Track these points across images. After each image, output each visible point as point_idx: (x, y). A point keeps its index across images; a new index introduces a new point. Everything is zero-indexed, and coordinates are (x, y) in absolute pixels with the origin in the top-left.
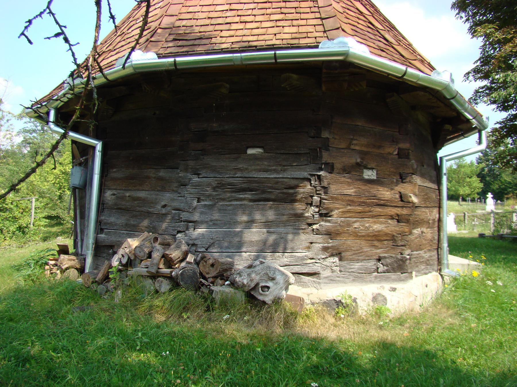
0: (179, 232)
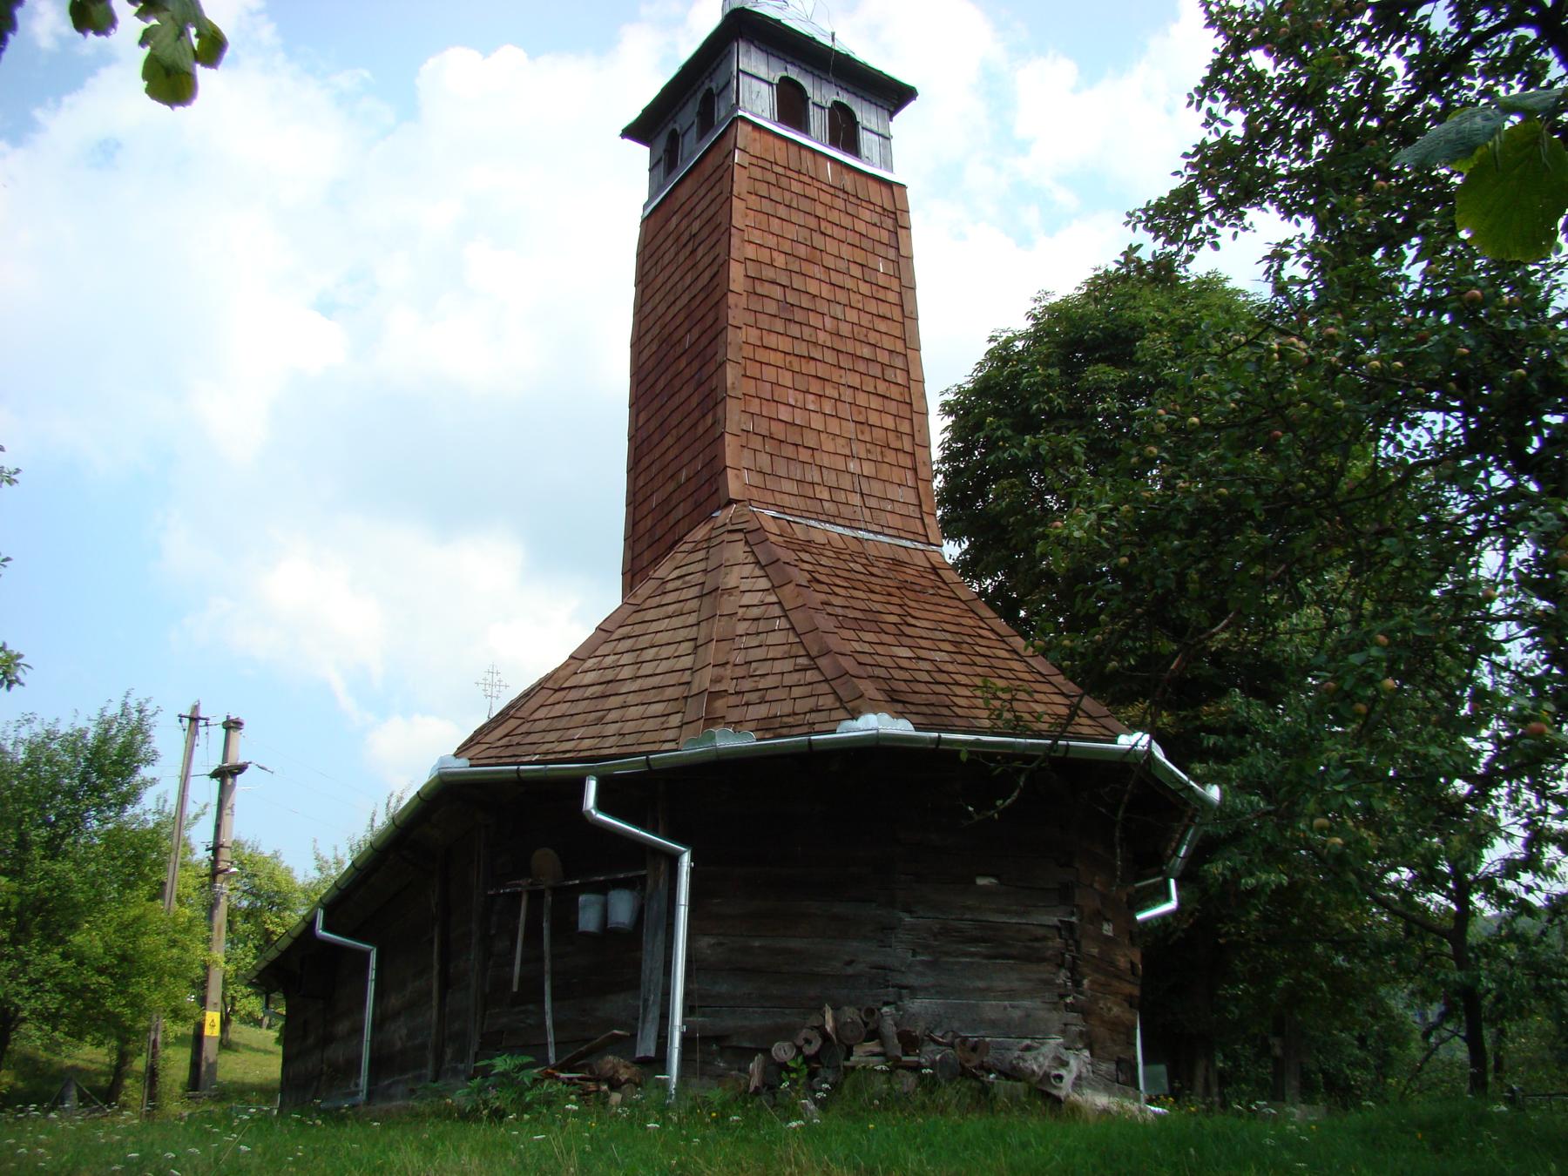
0: (886, 1004)
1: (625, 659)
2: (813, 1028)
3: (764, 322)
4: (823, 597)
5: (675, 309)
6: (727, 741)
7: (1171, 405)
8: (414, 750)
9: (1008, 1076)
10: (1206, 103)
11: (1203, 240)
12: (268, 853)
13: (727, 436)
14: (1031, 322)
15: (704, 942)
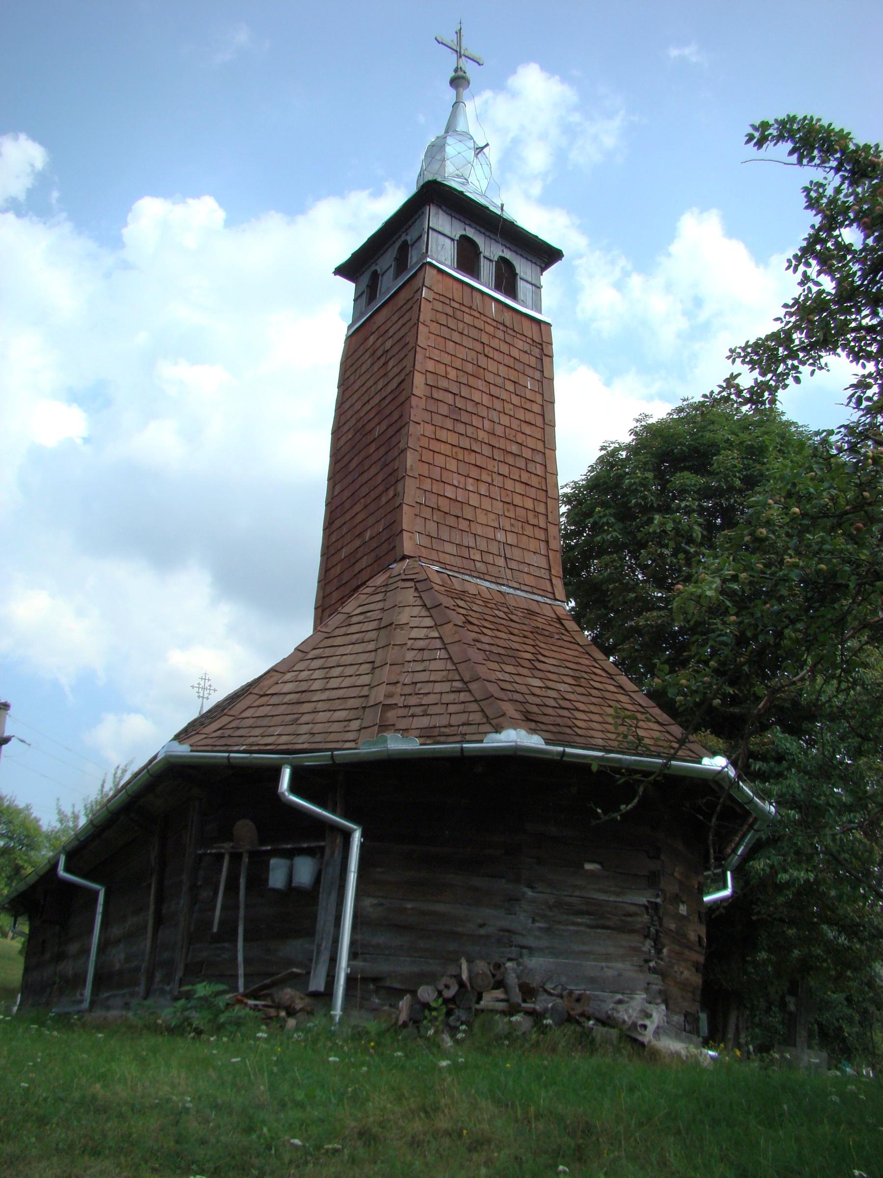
0: (510, 960)
1: (317, 674)
2: (452, 976)
3: (438, 420)
4: (474, 635)
5: (368, 407)
6: (397, 744)
7: (777, 497)
8: (137, 737)
9: (604, 1023)
10: (802, 268)
11: (788, 374)
12: (22, 805)
13: (405, 506)
14: (633, 437)
15: (368, 902)
